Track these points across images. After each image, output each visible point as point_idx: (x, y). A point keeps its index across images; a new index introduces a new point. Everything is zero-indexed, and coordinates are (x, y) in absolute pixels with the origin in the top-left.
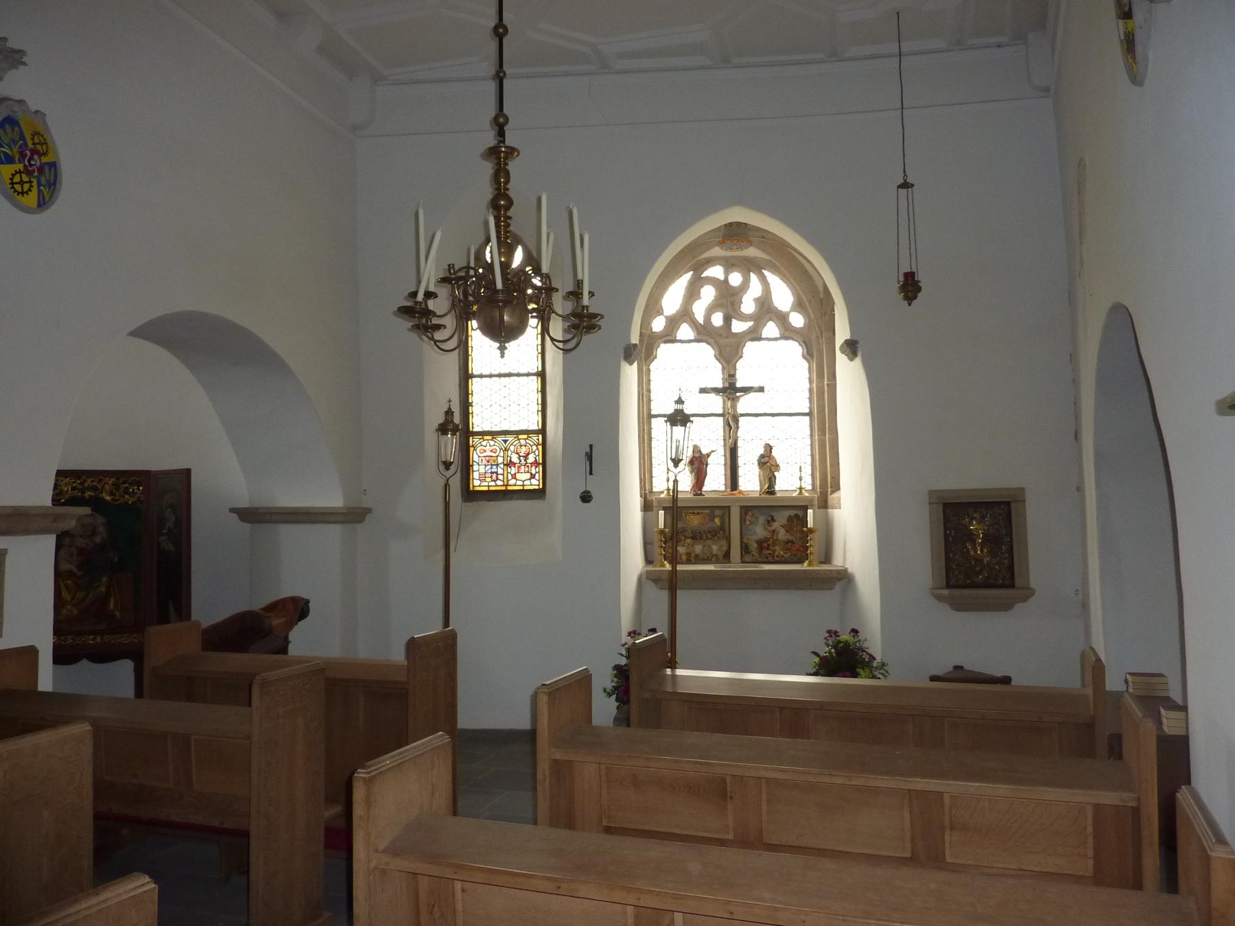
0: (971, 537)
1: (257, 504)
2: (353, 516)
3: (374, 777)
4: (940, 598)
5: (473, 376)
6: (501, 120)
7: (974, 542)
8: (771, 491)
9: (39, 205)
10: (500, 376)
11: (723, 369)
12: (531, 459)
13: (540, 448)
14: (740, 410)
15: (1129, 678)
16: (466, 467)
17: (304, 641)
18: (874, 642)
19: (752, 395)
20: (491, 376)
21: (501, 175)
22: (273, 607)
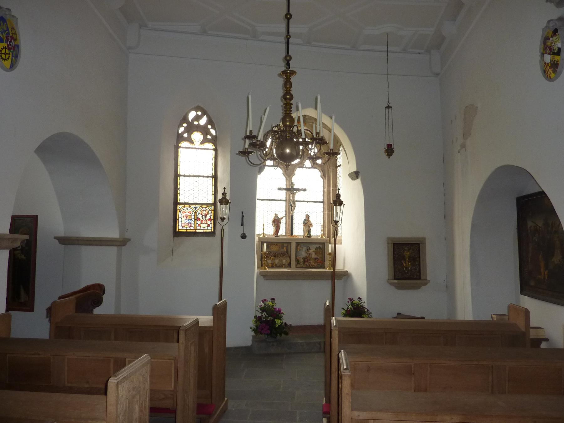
0: (404, 258)
1: (68, 235)
2: (122, 243)
4: (391, 284)
5: (180, 176)
6: (288, 58)
7: (405, 260)
8: (309, 236)
10: (194, 176)
11: (286, 180)
12: (208, 217)
13: (213, 212)
14: (296, 199)
15: (493, 316)
16: (175, 220)
18: (365, 303)
19: (301, 192)
20: (189, 176)
21: (288, 84)
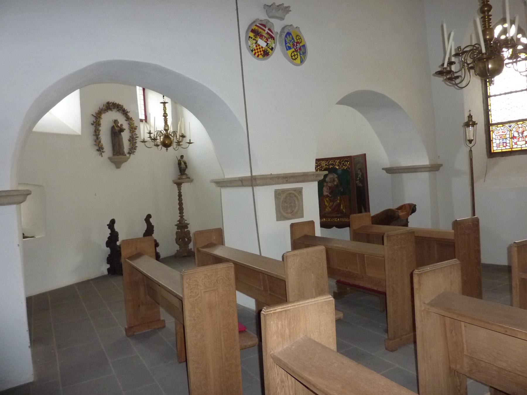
2: (434, 168)
3: (422, 273)
5: (490, 96)
9: (301, 62)
10: (505, 94)
16: (489, 141)
17: (415, 222)
22: (401, 208)
